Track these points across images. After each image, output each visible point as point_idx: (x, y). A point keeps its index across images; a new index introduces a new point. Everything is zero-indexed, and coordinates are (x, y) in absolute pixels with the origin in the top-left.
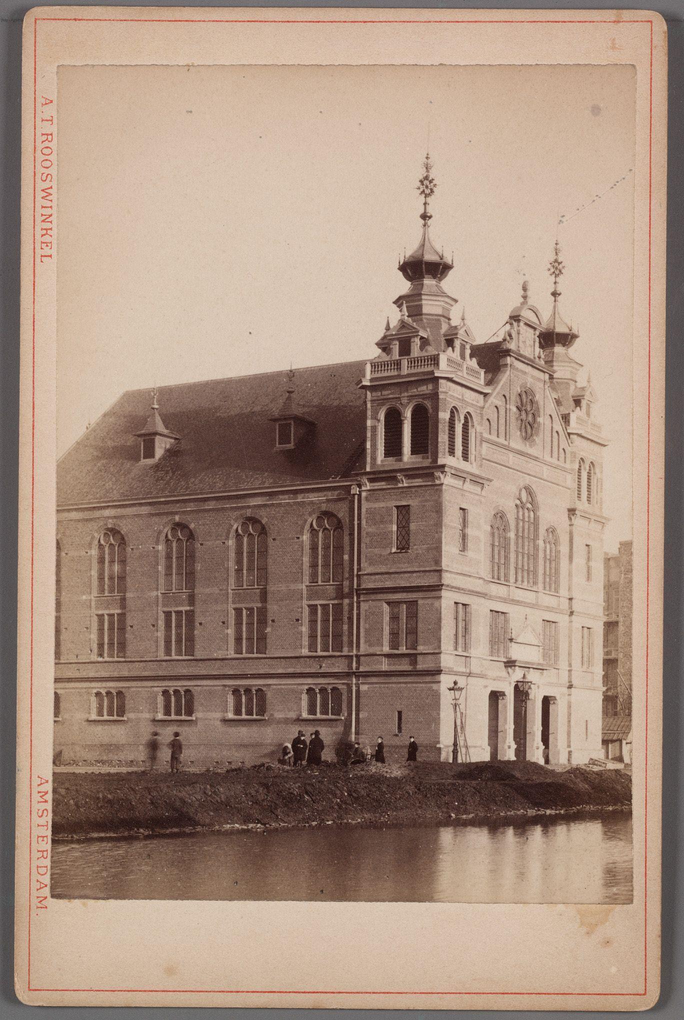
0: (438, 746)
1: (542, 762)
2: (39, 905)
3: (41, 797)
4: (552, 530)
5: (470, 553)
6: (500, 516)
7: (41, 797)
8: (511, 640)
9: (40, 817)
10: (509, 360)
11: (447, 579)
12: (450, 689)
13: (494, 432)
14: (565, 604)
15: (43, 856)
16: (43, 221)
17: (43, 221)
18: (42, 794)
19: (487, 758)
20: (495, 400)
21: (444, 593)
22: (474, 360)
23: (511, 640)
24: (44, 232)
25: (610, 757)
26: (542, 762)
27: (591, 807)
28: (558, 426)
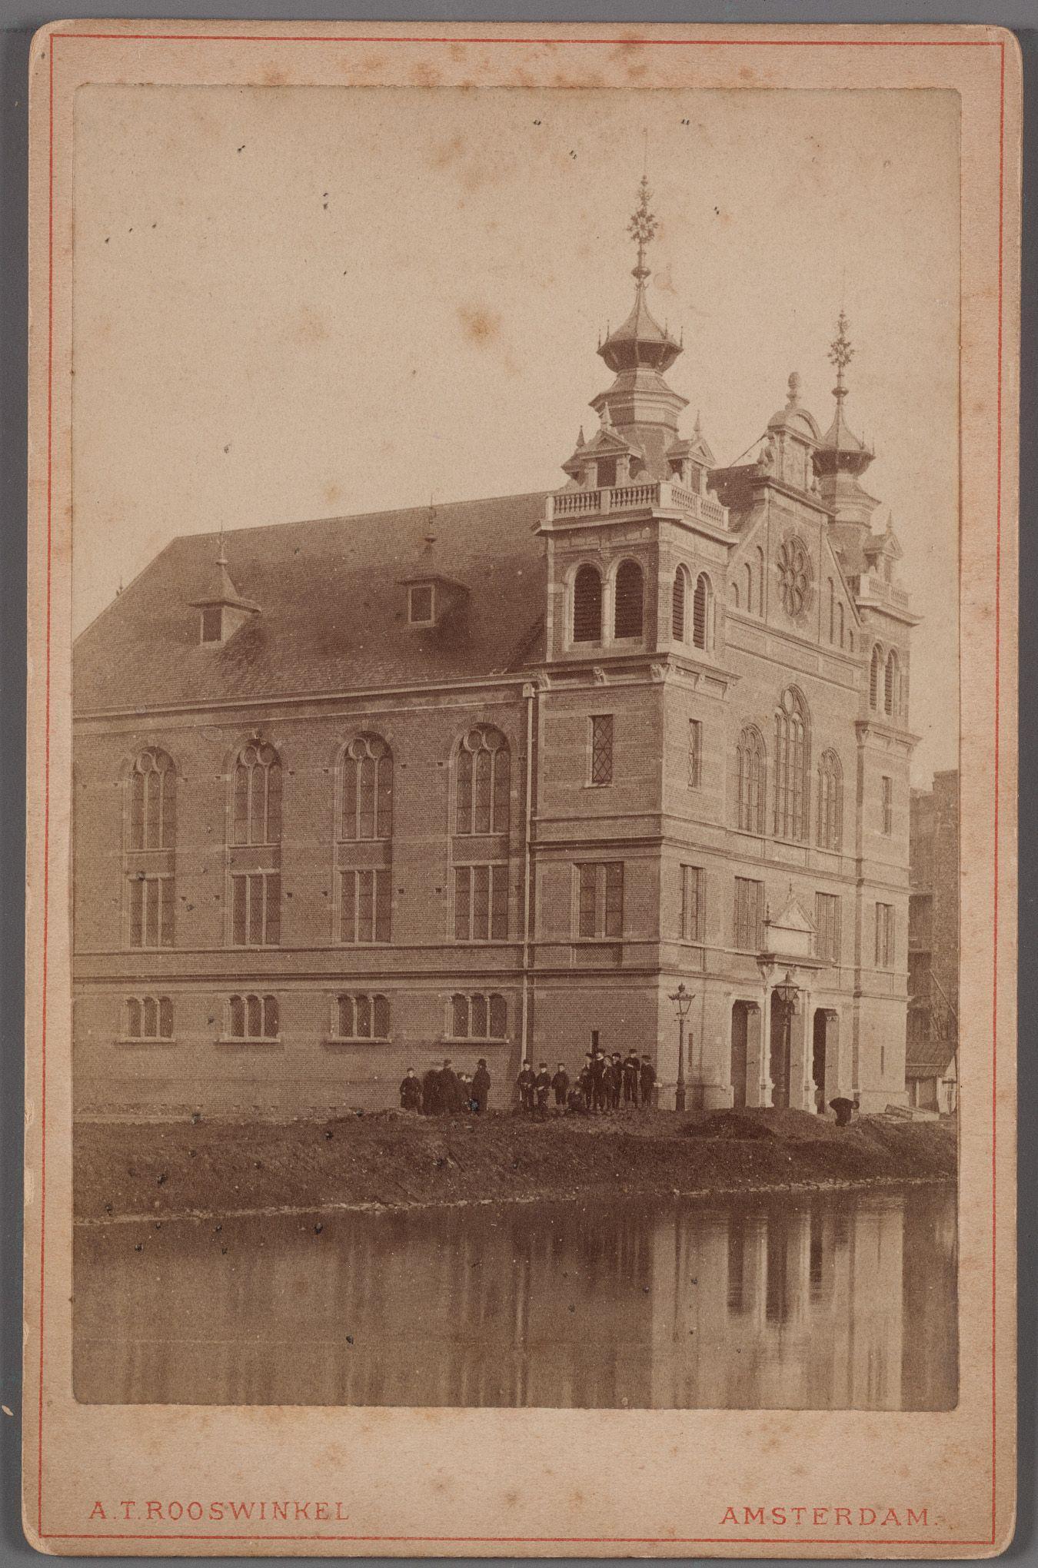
2: (921, 1521)
3: (754, 1518)
7: (754, 1518)
9: (784, 1521)
15: (157, 1510)
16: (284, 1516)
17: (284, 1516)
18: (750, 1518)
24: (301, 1514)
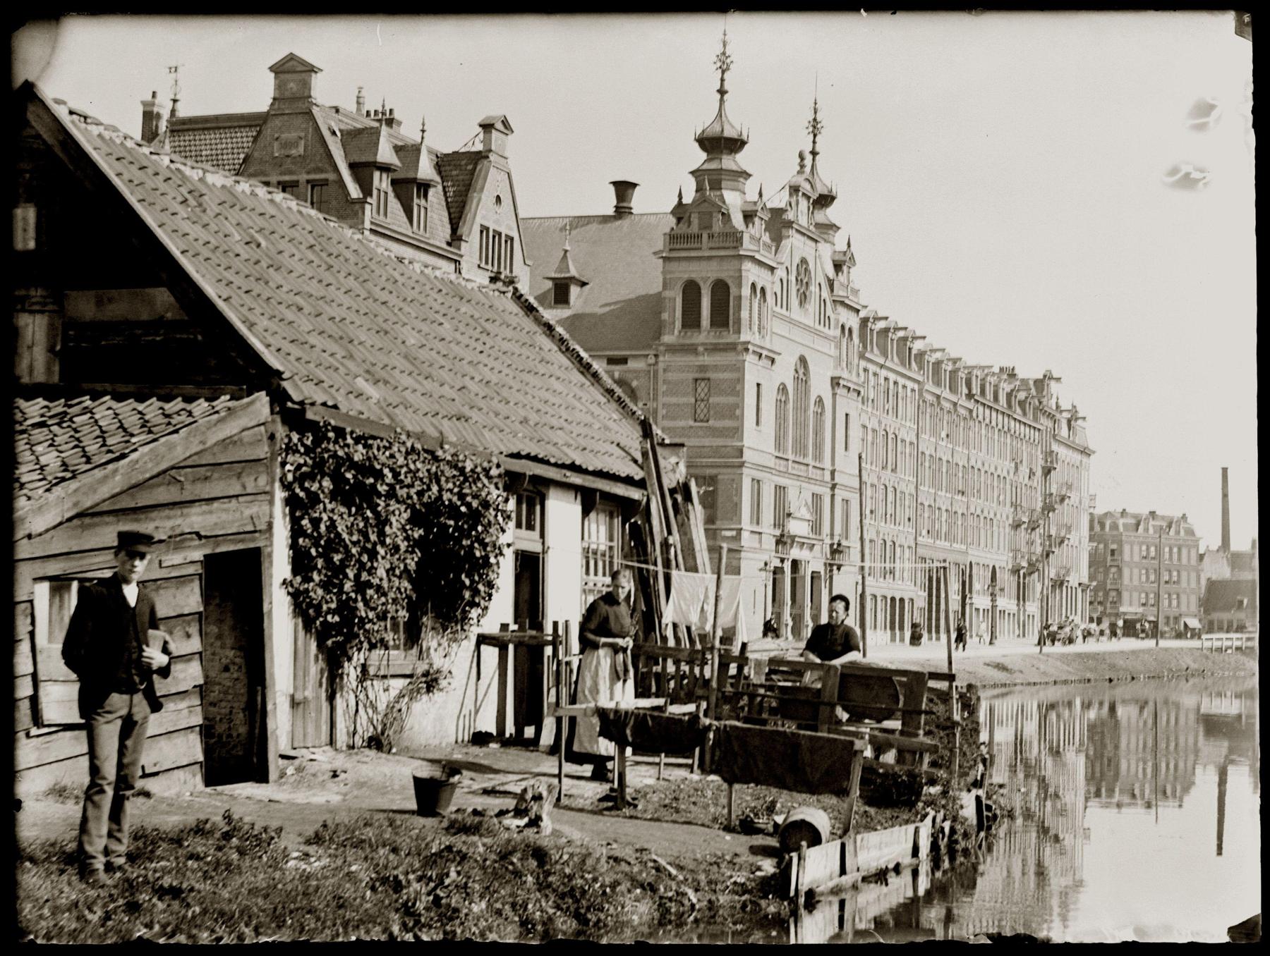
0: (144, 647)
1: (150, 732)
4: (820, 401)
5: (761, 427)
6: (783, 389)
8: (789, 515)
10: (791, 232)
11: (748, 455)
12: (761, 570)
13: (854, 373)
14: (828, 477)
19: (158, 694)
20: (781, 273)
21: (745, 470)
22: (767, 234)
23: (789, 515)
25: (342, 738)
26: (150, 732)
27: (316, 903)
28: (825, 293)
